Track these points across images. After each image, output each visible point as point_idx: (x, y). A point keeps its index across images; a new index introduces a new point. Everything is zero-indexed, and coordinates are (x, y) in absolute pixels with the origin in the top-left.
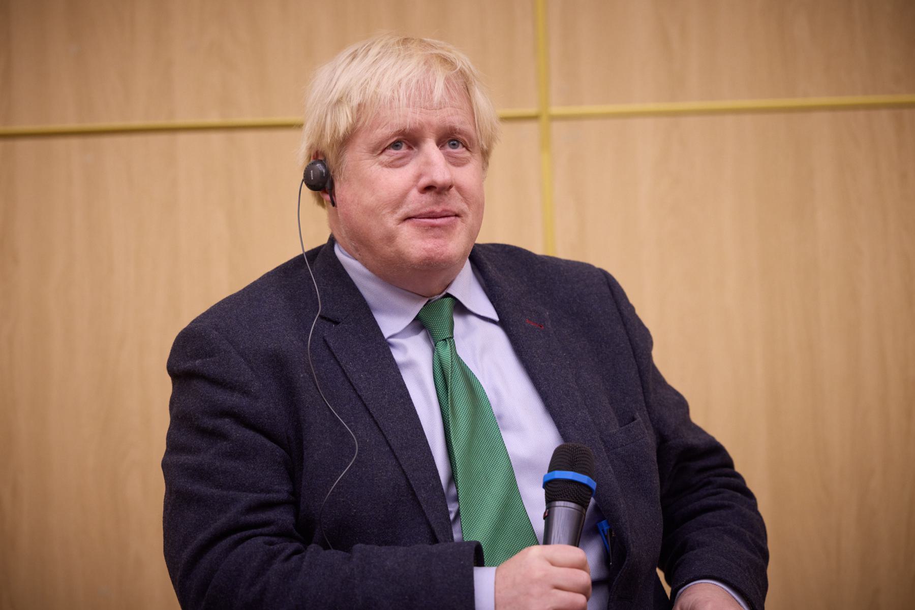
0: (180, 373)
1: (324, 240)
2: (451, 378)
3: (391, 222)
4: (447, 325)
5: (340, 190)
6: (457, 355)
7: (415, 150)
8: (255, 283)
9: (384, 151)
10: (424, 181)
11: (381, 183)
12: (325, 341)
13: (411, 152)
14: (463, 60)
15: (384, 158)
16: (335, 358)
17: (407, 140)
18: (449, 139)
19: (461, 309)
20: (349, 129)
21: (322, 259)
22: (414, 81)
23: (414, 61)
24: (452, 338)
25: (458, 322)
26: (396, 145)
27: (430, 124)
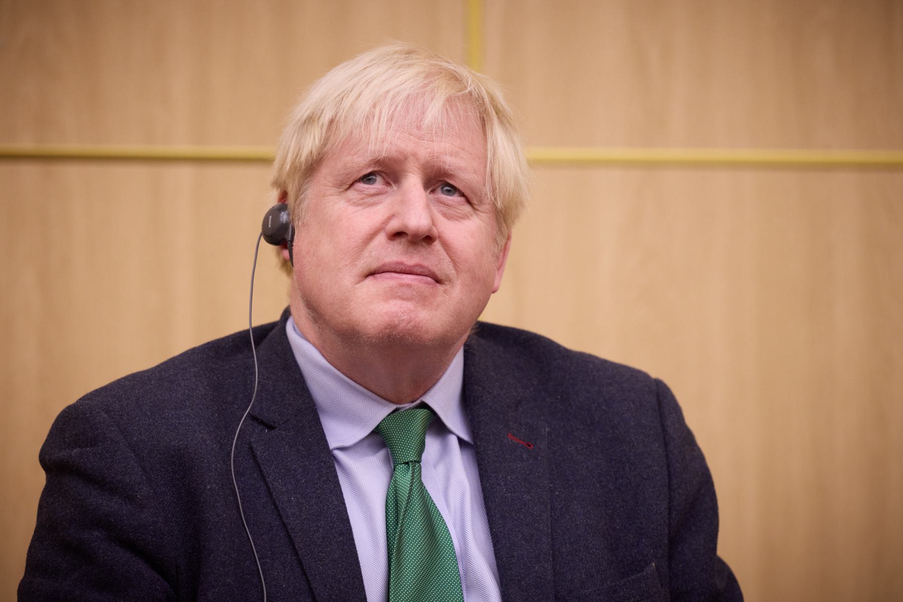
0: (49, 461)
1: (276, 317)
2: (409, 513)
3: (347, 279)
4: (414, 443)
5: (300, 243)
6: (421, 484)
7: (395, 188)
8: (173, 360)
9: (352, 185)
10: (394, 225)
11: (344, 224)
12: (251, 448)
13: (389, 189)
14: (473, 79)
15: (352, 194)
16: (261, 471)
17: (385, 172)
18: (439, 181)
19: (437, 426)
20: (315, 152)
21: (270, 338)
22: (404, 95)
23: (411, 72)
24: (419, 462)
25: (432, 445)
26: (367, 178)
27: (415, 155)
